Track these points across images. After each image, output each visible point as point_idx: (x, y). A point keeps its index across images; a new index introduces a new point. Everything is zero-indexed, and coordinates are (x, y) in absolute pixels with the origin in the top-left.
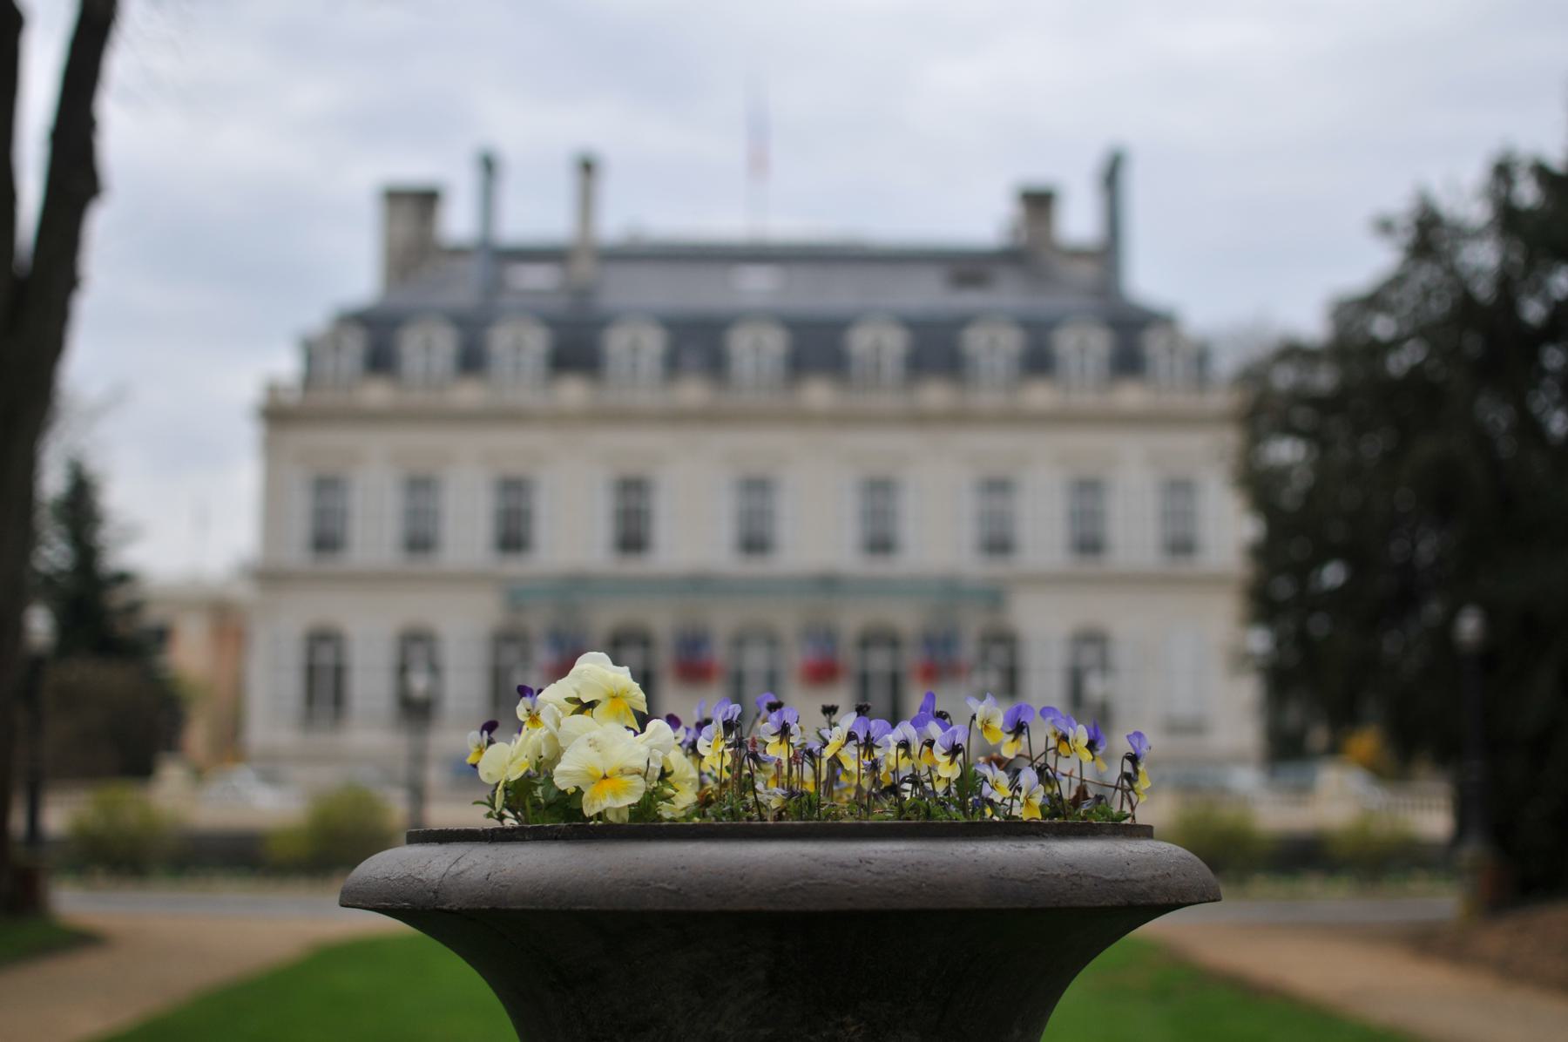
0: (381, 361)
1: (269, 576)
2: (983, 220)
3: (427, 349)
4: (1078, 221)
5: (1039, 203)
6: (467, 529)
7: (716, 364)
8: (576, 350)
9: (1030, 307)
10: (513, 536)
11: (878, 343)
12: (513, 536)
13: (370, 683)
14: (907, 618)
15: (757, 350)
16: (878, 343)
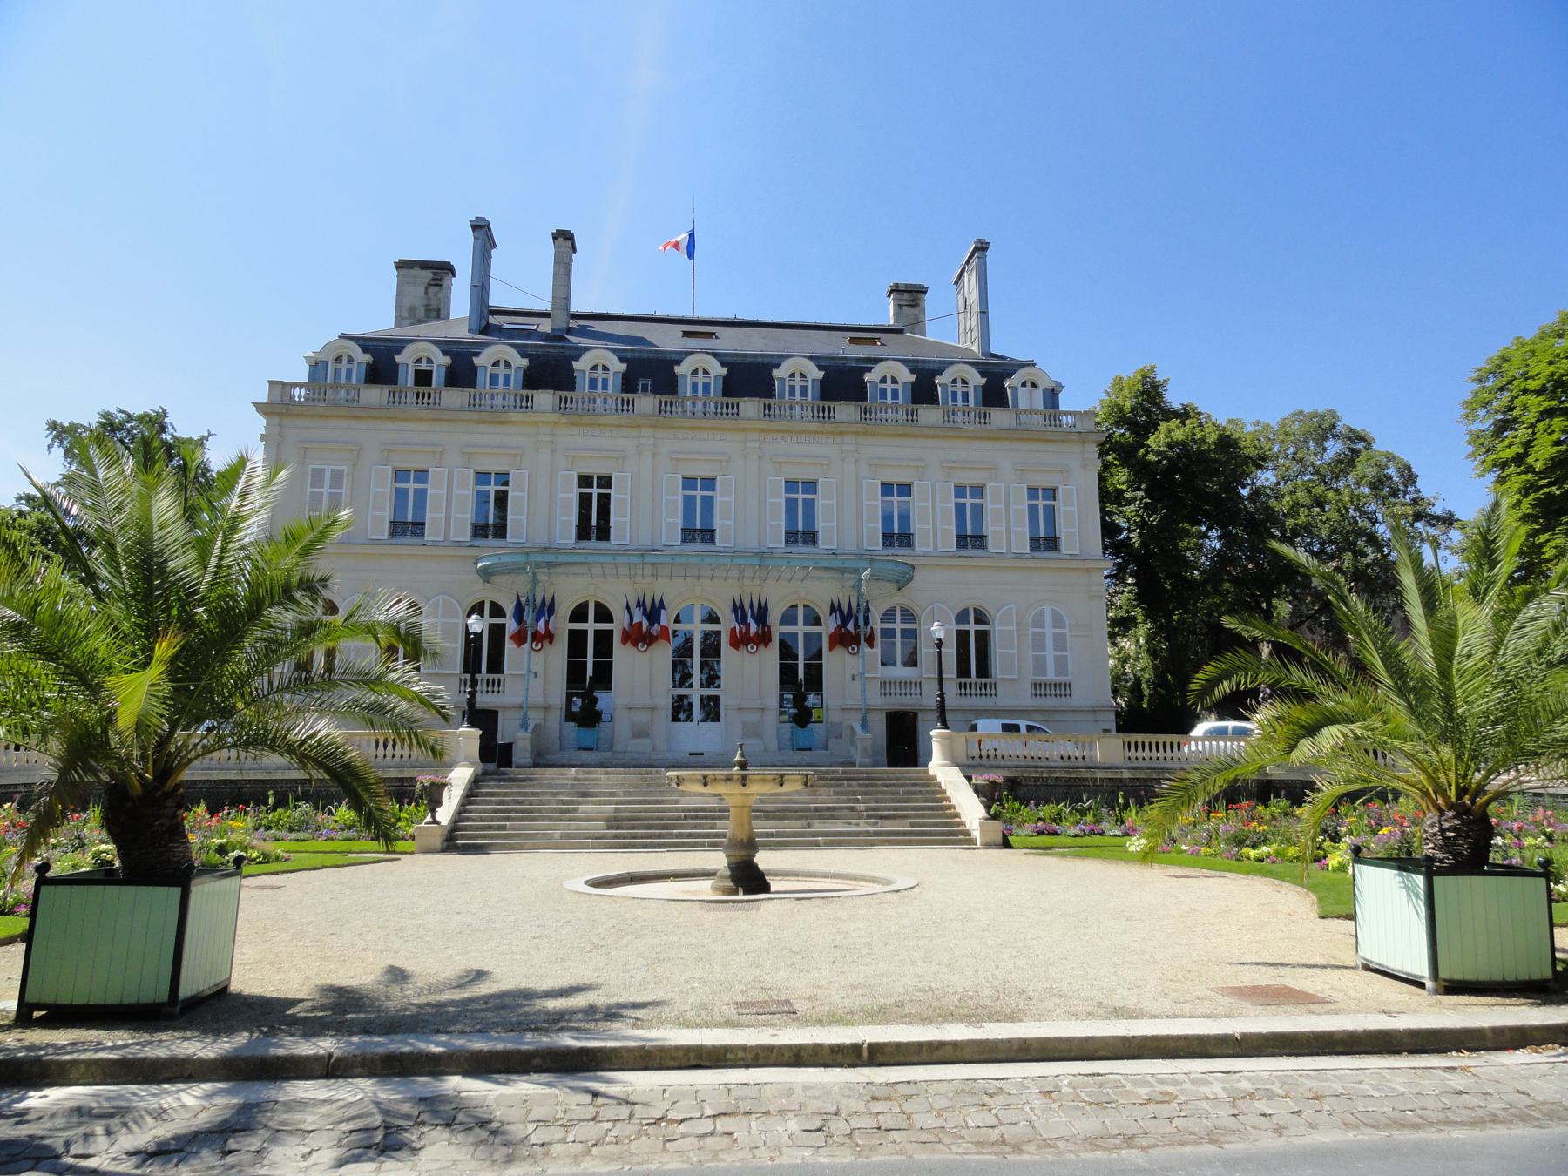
10: (491, 527)
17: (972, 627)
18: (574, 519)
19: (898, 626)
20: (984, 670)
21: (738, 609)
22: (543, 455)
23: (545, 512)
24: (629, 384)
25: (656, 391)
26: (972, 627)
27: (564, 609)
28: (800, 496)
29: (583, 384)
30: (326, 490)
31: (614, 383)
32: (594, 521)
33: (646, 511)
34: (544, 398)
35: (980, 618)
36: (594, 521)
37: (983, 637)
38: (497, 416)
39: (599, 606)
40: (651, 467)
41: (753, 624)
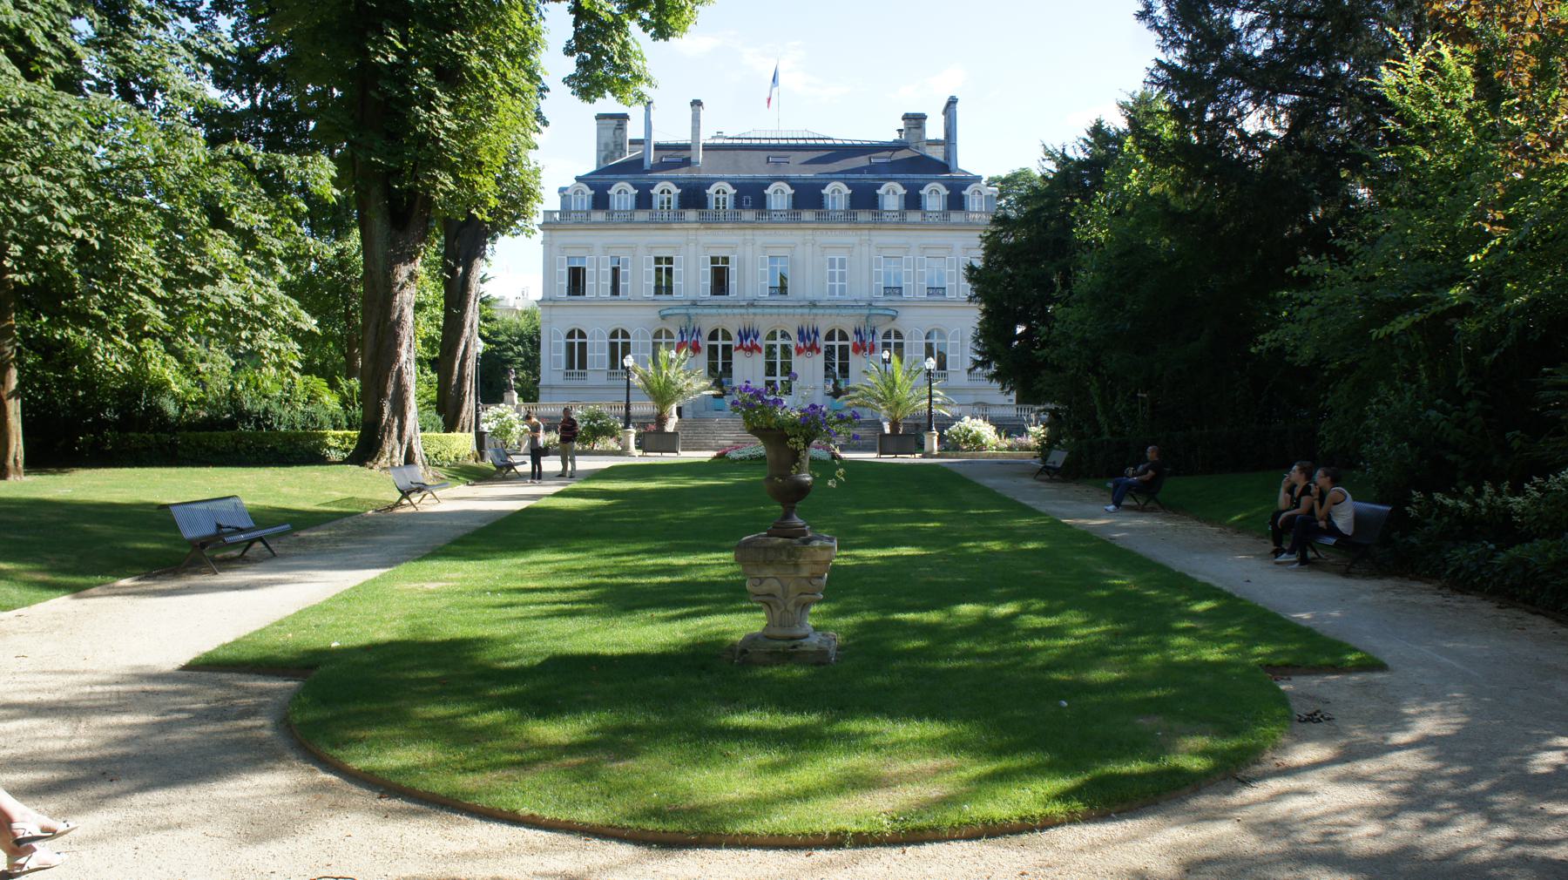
0: (601, 201)
1: (547, 302)
2: (888, 131)
3: (623, 193)
4: (934, 129)
5: (915, 121)
6: (640, 279)
7: (760, 203)
8: (751, 196)
9: (906, 171)
10: (664, 285)
11: (721, 191)
12: (664, 285)
13: (598, 353)
14: (848, 323)
15: (779, 196)
16: (721, 191)
17: (620, 340)
18: (653, 283)
19: (893, 341)
20: (583, 365)
21: (800, 332)
22: (693, 247)
23: (692, 280)
24: (738, 203)
25: (753, 208)
26: (576, 340)
27: (764, 334)
28: (664, 266)
29: (712, 204)
30: (837, 270)
31: (730, 203)
32: (720, 281)
33: (750, 280)
34: (691, 214)
35: (582, 335)
36: (720, 281)
37: (583, 346)
38: (665, 224)
39: (841, 332)
40: (755, 252)
41: (808, 340)
